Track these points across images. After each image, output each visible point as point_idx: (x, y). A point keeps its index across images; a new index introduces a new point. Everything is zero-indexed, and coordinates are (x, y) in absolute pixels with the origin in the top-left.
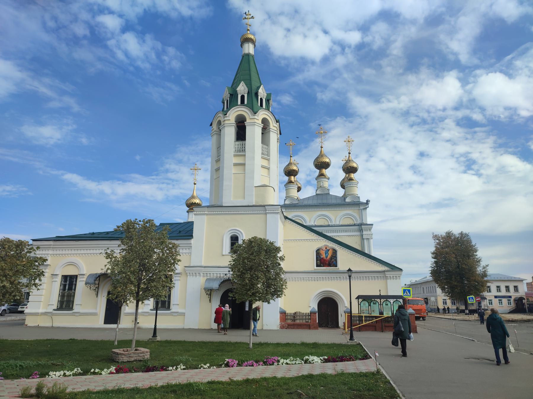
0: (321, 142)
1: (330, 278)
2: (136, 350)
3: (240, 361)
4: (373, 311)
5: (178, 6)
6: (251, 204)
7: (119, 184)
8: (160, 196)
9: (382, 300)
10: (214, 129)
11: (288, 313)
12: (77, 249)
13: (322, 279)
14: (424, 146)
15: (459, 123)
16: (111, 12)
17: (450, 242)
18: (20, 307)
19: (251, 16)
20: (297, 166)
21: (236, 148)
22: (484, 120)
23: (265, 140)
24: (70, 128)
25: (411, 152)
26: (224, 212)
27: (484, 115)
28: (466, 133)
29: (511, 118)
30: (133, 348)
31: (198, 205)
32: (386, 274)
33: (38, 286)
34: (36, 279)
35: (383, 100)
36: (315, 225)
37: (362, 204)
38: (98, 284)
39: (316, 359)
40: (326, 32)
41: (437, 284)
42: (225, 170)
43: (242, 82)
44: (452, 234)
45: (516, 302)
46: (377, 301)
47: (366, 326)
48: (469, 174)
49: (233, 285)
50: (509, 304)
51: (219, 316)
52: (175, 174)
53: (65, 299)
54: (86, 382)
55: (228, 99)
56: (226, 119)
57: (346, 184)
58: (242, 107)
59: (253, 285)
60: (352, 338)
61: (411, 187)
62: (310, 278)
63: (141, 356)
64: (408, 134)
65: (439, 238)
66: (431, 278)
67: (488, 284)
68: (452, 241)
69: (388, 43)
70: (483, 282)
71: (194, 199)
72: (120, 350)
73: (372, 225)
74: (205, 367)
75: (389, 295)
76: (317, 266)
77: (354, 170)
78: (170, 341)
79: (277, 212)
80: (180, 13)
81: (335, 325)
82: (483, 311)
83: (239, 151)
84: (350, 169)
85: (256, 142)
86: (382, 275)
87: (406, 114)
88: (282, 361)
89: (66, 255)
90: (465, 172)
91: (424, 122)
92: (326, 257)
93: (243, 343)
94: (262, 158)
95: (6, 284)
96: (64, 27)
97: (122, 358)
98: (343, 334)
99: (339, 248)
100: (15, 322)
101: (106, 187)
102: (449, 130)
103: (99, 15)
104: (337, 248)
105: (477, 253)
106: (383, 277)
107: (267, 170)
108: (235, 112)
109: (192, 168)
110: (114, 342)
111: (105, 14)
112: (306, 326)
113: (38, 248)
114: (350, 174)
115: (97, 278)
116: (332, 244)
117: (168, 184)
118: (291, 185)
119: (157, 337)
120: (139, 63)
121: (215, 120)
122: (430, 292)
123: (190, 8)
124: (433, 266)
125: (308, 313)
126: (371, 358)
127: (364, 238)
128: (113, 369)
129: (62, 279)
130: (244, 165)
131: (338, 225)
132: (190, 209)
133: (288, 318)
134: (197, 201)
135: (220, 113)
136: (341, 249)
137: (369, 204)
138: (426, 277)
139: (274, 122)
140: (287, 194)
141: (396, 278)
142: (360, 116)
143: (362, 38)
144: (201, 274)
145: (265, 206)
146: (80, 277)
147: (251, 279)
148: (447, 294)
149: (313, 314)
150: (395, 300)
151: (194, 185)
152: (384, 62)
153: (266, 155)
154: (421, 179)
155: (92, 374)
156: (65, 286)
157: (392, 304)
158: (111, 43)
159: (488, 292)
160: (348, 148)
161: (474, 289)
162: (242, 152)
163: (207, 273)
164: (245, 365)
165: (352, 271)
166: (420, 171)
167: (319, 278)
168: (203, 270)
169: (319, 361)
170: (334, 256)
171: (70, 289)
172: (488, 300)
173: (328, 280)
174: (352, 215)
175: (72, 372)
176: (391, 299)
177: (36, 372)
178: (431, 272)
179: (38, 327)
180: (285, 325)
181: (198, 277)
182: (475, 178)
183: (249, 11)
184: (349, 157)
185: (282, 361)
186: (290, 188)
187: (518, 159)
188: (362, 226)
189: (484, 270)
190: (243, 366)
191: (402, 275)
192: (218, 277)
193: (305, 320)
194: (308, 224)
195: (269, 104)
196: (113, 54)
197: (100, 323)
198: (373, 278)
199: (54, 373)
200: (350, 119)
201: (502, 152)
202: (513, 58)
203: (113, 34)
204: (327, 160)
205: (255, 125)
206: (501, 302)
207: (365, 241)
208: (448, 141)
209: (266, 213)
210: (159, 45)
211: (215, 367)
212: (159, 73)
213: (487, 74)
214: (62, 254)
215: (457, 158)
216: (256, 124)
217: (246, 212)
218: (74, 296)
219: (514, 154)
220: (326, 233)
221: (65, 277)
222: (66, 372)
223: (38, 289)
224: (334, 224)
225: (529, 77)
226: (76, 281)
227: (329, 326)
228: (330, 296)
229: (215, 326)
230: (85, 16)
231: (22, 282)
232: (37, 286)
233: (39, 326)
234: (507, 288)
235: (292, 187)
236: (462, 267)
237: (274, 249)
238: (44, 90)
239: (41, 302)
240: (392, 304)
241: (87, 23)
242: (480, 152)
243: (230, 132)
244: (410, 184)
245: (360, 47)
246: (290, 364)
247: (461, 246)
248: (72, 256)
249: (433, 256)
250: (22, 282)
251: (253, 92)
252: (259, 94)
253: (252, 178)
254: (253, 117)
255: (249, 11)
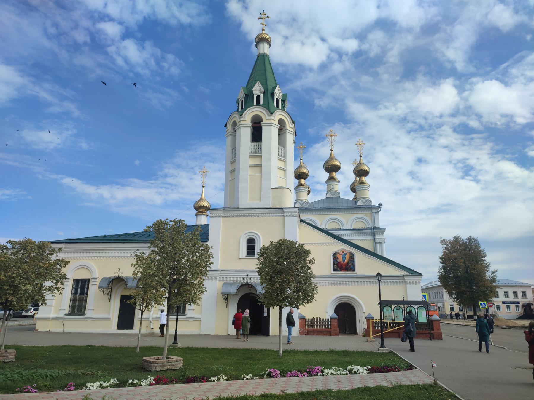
0: (333, 146)
1: (348, 282)
2: (167, 358)
3: (281, 371)
4: (397, 317)
5: (177, 13)
6: (268, 207)
7: (118, 188)
8: (158, 200)
9: (406, 306)
10: (228, 130)
11: (307, 319)
12: (89, 251)
13: (339, 284)
14: (422, 152)
15: (456, 129)
16: (111, 19)
17: (458, 247)
18: (24, 311)
19: (266, 16)
20: (306, 169)
21: (252, 149)
22: (481, 127)
23: (282, 142)
24: (70, 133)
25: (409, 158)
26: (241, 215)
27: (481, 122)
28: (463, 140)
29: (507, 125)
30: (165, 356)
31: (207, 208)
32: (405, 278)
33: (61, 290)
34: (58, 282)
35: (381, 106)
36: (327, 229)
37: (375, 207)
38: (111, 288)
39: (360, 369)
40: (323, 40)
41: (446, 289)
42: (241, 171)
43: (258, 82)
44: (461, 239)
45: (525, 308)
46: (400, 307)
47: (391, 332)
48: (467, 179)
49: (250, 290)
50: (517, 310)
51: (237, 322)
52: (174, 179)
53: (77, 303)
54: (129, 394)
55: (244, 99)
56: (241, 119)
57: (357, 188)
58: (258, 108)
59: (283, 290)
60: (382, 346)
61: (409, 192)
62: (327, 283)
63: (174, 364)
64: (406, 139)
65: (447, 242)
66: (438, 283)
67: (497, 290)
68: (460, 246)
69: (384, 51)
70: (492, 288)
71: (202, 202)
72: (151, 358)
73: (385, 229)
74: (248, 377)
75: (409, 300)
76: (334, 270)
77: (365, 173)
78: (192, 347)
79: (295, 215)
80: (179, 21)
81: (353, 331)
82: (492, 317)
83: (255, 152)
84: (361, 173)
85: (272, 142)
86: (401, 280)
87: (403, 120)
88: (326, 371)
89: (78, 258)
90: (463, 178)
91: (421, 128)
92: (344, 261)
93: (269, 350)
94: (278, 159)
95: (29, 288)
96: (65, 33)
97: (155, 366)
98: (367, 341)
99: (356, 251)
100: (23, 326)
101: (105, 191)
102: (447, 136)
103: (99, 22)
104: (354, 252)
105: (486, 258)
106: (402, 281)
107: (283, 172)
108: (253, 112)
109: (200, 171)
110: (136, 348)
111: (105, 21)
112: (326, 332)
113: (60, 249)
114: (362, 177)
115: (111, 282)
116: (349, 248)
117: (167, 188)
118: (302, 188)
119: (178, 343)
120: (139, 70)
121: (229, 121)
122: (436, 298)
123: (189, 15)
124: (441, 272)
125: (329, 319)
126: (416, 368)
127: (376, 242)
128: (151, 379)
129: (74, 283)
130: (260, 166)
131: (350, 229)
132: (198, 212)
133: (307, 324)
134: (206, 204)
135: (236, 113)
136: (359, 253)
137: (381, 207)
138: (431, 283)
139: (290, 123)
140: (297, 196)
141: (416, 284)
142: (357, 122)
143: (360, 46)
144: (218, 278)
145: (282, 208)
146: (93, 281)
147: (281, 283)
148: (456, 299)
149: (333, 320)
150: (419, 305)
151: (202, 188)
152: (381, 70)
153: (282, 157)
154: (419, 185)
155: (131, 385)
156: (76, 290)
157: (416, 310)
158: (111, 49)
159: (495, 298)
160: (359, 150)
161: (483, 294)
162: (258, 154)
163: (223, 277)
164: (289, 375)
165: (381, 275)
166: (418, 177)
167: (336, 283)
168: (219, 274)
169: (365, 371)
170: (351, 260)
171: (82, 293)
172: (495, 306)
173: (345, 285)
174: (364, 219)
175: (109, 383)
176: (415, 305)
177: (71, 383)
178: (439, 277)
179: (49, 332)
180: (304, 331)
181: (214, 281)
182: (473, 184)
183: (264, 11)
184: (360, 160)
185: (326, 371)
186: (301, 191)
187: (516, 165)
188: (374, 230)
189: (492, 275)
190: (287, 376)
191: (422, 278)
192: (235, 281)
193: (326, 326)
194: (323, 227)
195: (284, 104)
196: (113, 61)
197: (113, 329)
198: (392, 283)
199: (92, 384)
200: (348, 125)
201: (500, 158)
202: (508, 66)
203: (113, 40)
204: (337, 163)
205: (272, 125)
206: (509, 308)
207: (378, 245)
208: (445, 147)
209: (284, 215)
210: (159, 52)
211: (258, 378)
212: (158, 79)
213: (483, 82)
214: (74, 257)
215: (455, 164)
216: (272, 124)
217: (263, 214)
218: (86, 300)
219: (511, 160)
220: (344, 236)
221: (77, 281)
222: (102, 382)
223: (61, 293)
224: (346, 227)
225: (525, 85)
226: (88, 285)
227: (346, 332)
228: (350, 302)
229: (232, 331)
230: (86, 23)
231: (45, 286)
232: (59, 290)
233: (50, 331)
234: (515, 294)
235: (304, 190)
236: (470, 272)
237: (304, 252)
238: (44, 95)
239: (52, 306)
240: (416, 310)
241: (87, 29)
242: (478, 158)
243: (245, 133)
244: (409, 190)
245: (357, 54)
246: (335, 375)
247: (469, 251)
248: (102, 258)
249: (441, 261)
250: (45, 286)
251: (269, 92)
252: (275, 95)
253: (269, 180)
254: (270, 118)
255: (264, 11)
